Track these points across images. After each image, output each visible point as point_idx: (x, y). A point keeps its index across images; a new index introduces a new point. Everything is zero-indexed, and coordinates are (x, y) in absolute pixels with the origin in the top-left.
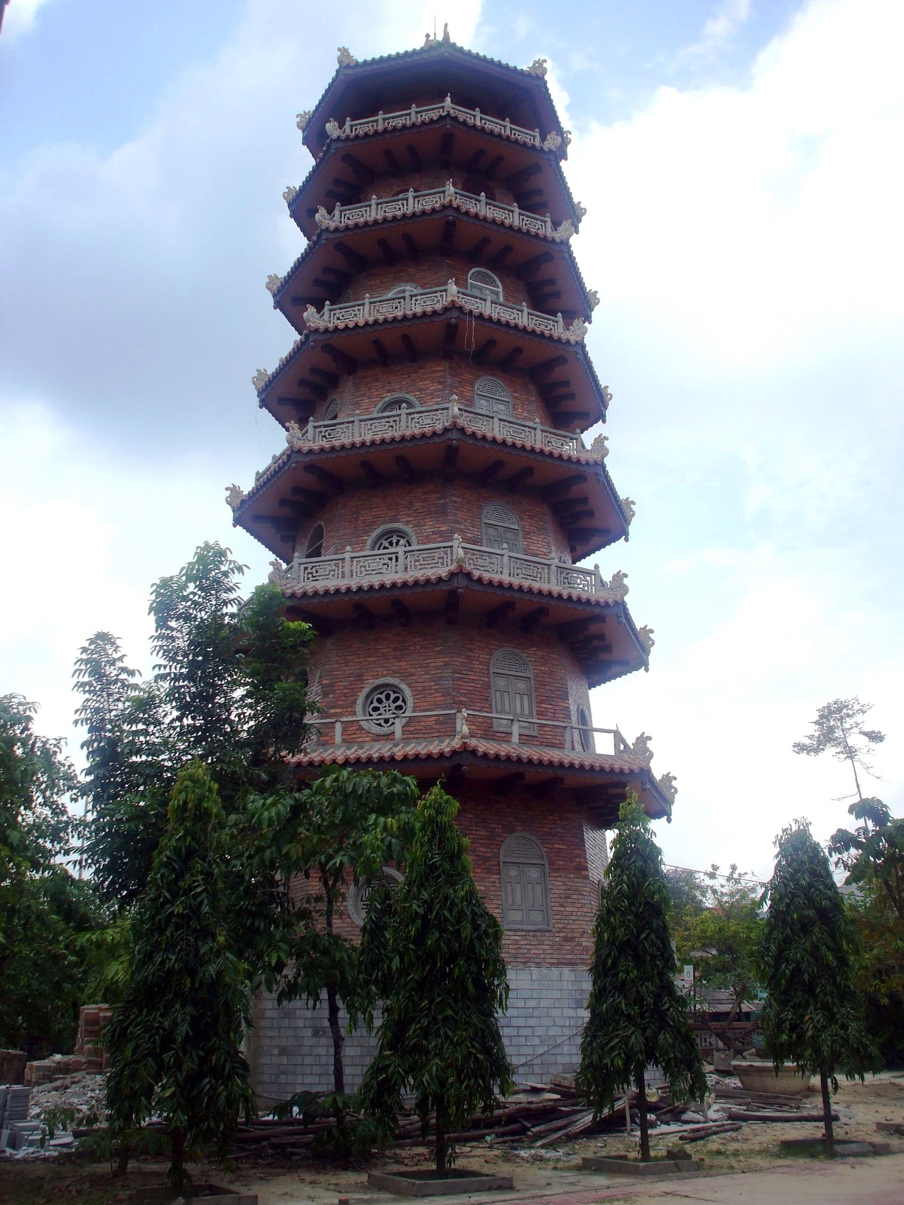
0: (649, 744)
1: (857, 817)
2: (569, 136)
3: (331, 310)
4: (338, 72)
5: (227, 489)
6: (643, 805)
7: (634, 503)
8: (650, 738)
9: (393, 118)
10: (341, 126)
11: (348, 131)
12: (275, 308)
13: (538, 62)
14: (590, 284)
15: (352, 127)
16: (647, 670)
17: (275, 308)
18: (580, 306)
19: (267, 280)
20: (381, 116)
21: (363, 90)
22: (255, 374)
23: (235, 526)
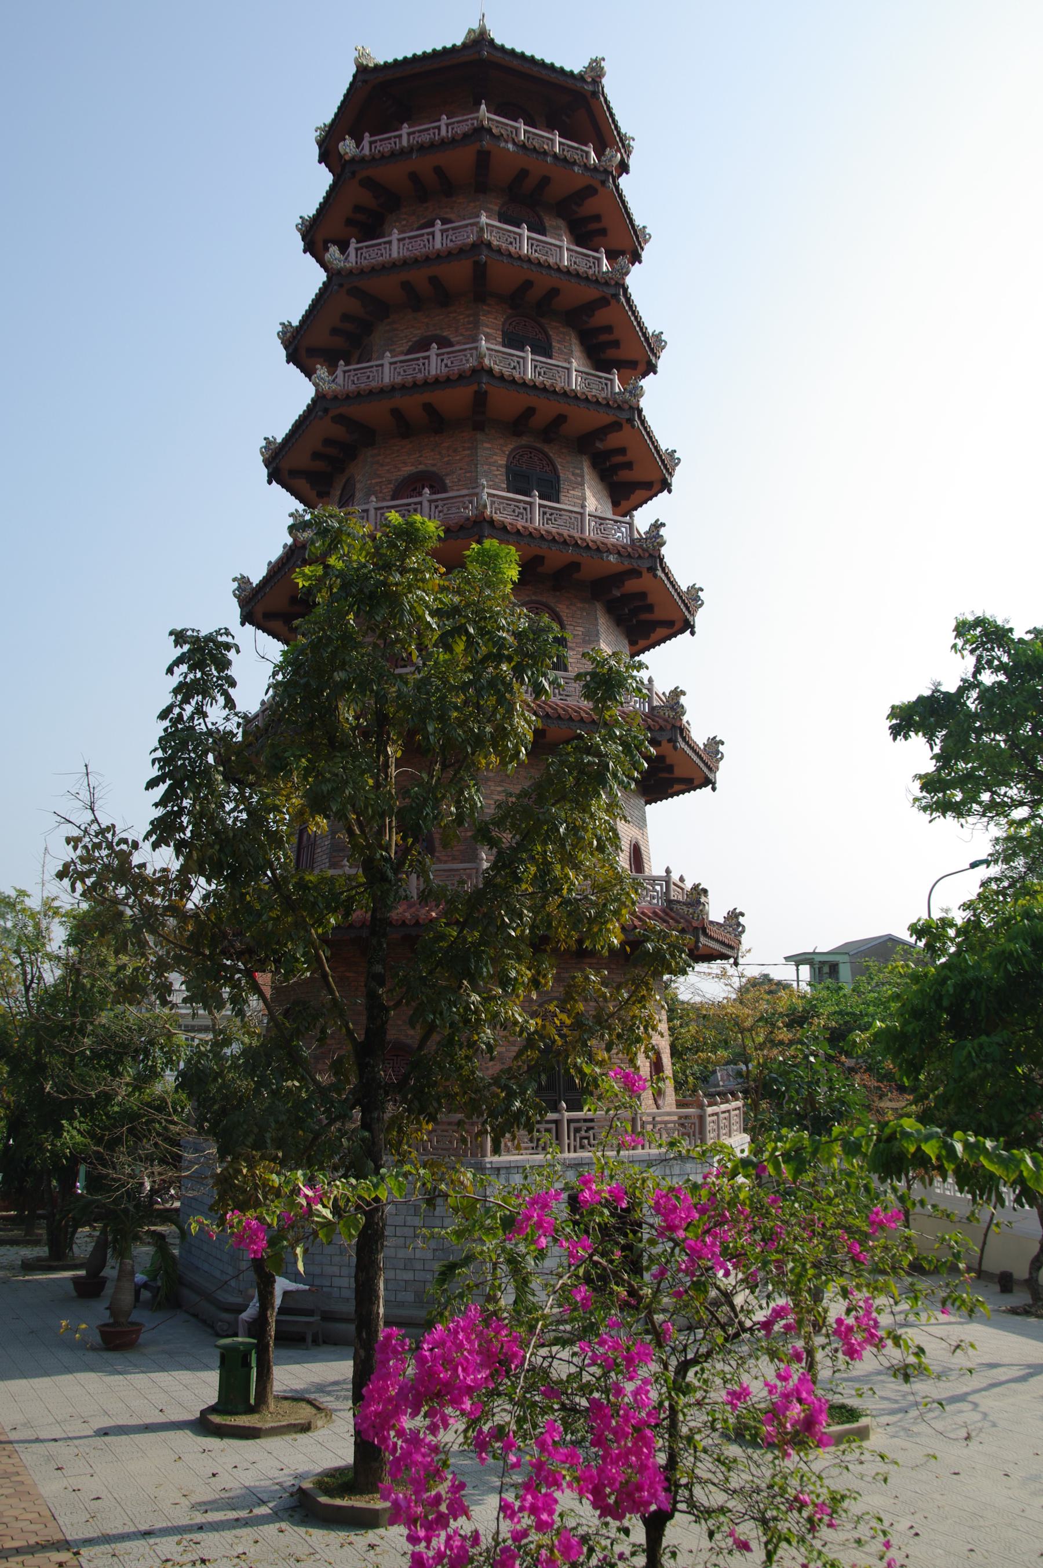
0: (663, 531)
1: (922, 789)
2: (632, 143)
3: (345, 372)
4: (355, 76)
5: (234, 580)
6: (748, 1437)
7: (742, 914)
8: (663, 525)
9: (420, 131)
10: (358, 145)
11: (366, 151)
12: (288, 362)
13: (596, 61)
14: (652, 326)
15: (371, 143)
16: (670, 491)
17: (288, 362)
18: (629, 245)
19: (280, 328)
20: (405, 129)
21: (382, 96)
22: (264, 443)
23: (270, 482)
